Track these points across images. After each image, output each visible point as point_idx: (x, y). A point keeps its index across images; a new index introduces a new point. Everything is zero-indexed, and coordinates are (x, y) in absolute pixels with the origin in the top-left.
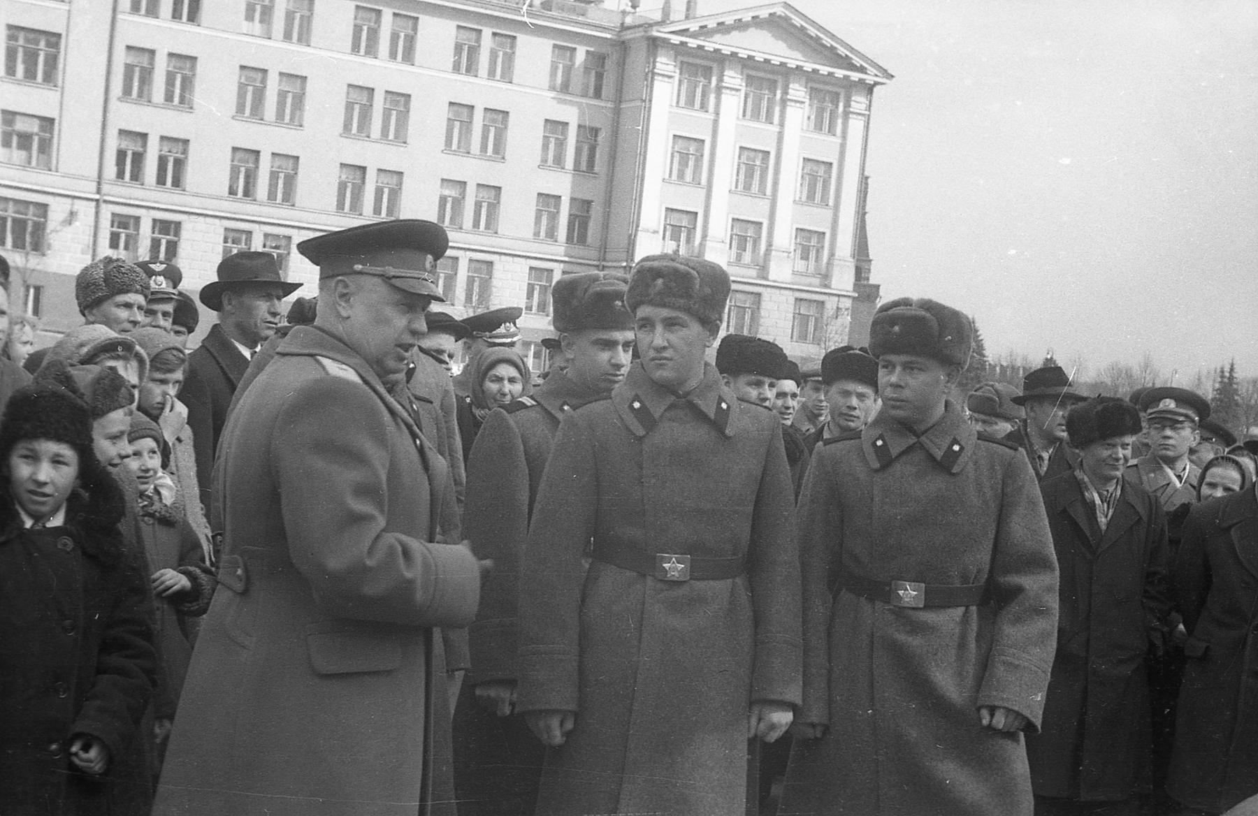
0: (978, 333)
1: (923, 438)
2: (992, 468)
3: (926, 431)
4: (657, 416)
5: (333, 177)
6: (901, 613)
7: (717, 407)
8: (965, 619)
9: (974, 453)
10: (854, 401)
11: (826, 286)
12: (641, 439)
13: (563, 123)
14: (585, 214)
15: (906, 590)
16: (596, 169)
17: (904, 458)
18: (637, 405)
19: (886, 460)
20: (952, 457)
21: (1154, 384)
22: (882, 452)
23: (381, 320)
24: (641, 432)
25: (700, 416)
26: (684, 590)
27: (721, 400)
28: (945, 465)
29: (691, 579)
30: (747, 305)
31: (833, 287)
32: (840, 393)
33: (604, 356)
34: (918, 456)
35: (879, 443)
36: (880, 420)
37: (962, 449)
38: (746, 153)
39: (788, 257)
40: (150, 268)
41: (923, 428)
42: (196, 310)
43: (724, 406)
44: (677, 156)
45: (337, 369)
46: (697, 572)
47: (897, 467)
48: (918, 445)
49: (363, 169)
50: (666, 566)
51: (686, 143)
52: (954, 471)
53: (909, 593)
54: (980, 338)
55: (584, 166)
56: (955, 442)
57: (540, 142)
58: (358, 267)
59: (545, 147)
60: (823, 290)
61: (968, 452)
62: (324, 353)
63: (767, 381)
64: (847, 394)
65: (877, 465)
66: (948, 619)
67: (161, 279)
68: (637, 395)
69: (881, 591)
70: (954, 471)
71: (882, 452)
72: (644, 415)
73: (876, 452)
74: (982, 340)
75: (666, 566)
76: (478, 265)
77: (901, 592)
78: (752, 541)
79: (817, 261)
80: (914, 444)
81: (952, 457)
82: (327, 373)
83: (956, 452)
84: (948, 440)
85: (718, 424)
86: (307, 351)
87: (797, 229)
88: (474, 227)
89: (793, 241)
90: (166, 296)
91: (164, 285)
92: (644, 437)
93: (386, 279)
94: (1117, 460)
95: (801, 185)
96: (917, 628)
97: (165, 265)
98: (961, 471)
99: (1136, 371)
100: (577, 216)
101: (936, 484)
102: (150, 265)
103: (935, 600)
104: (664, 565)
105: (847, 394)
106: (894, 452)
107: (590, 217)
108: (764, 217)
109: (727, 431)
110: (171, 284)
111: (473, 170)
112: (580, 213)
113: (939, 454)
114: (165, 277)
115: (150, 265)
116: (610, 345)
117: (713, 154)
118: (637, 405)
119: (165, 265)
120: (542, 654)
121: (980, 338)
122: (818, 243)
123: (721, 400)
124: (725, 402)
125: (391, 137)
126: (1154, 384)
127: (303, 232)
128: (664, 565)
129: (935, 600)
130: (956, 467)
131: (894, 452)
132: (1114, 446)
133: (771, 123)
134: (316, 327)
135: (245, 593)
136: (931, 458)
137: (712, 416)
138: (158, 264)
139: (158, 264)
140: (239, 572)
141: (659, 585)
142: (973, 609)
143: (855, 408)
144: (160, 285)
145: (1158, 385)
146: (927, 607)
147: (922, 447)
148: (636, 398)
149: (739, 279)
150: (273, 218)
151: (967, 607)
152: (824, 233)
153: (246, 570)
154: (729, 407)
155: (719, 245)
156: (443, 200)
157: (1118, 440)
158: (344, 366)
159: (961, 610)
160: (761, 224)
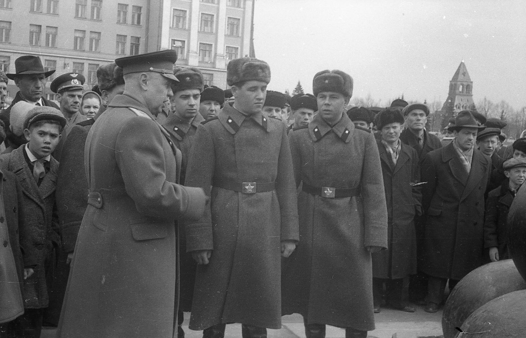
0: (302, 87)
1: (333, 128)
2: (361, 140)
3: (334, 126)
4: (239, 125)
5: (27, 30)
6: (326, 200)
7: (262, 121)
8: (350, 202)
9: (353, 134)
10: (307, 116)
11: (214, 68)
12: (233, 135)
13: (126, 5)
14: (137, 43)
15: (328, 190)
16: (141, 24)
17: (326, 137)
18: (230, 121)
19: (319, 137)
20: (345, 136)
21: (372, 105)
22: (317, 134)
23: (160, 91)
24: (233, 132)
25: (256, 124)
26: (254, 197)
27: (263, 117)
28: (343, 139)
29: (256, 192)
30: (208, 79)
31: (216, 67)
32: (301, 113)
33: (185, 102)
34: (331, 136)
35: (316, 130)
36: (314, 121)
37: (349, 132)
38: (205, 15)
39: (223, 58)
40: (70, 76)
41: (334, 123)
42: (53, 92)
43: (265, 120)
44: (175, 17)
45: (140, 113)
46: (258, 189)
47: (323, 141)
48: (331, 131)
49: (40, 26)
50: (247, 187)
51: (207, 16)
52: (346, 142)
53: (329, 192)
54: (302, 89)
55: (136, 23)
56: (346, 129)
57: (116, 13)
58: (151, 69)
59: (119, 15)
60: (213, 69)
61: (351, 134)
62: (132, 106)
63: (274, 108)
64: (304, 113)
65: (316, 139)
66: (343, 202)
67: (76, 80)
68: (229, 117)
69: (317, 191)
70: (346, 142)
71: (317, 134)
72: (233, 125)
73: (343, 133)
74: (303, 90)
75: (247, 187)
76: (77, 65)
77: (326, 192)
78: (278, 175)
79: (209, 56)
80: (330, 130)
81: (345, 136)
82: (137, 115)
83: (347, 134)
84: (344, 129)
85: (263, 128)
86: (124, 106)
87: (227, 47)
88: (90, 49)
89: (225, 52)
90: (78, 88)
91: (78, 83)
92: (235, 134)
93: (162, 73)
94: (391, 134)
95: (228, 28)
96: (333, 207)
97: (77, 74)
98: (349, 142)
99: (365, 101)
100: (134, 44)
101: (339, 147)
102: (71, 75)
103: (339, 194)
104: (246, 187)
105: (304, 113)
106: (323, 134)
107: (139, 44)
108: (239, 46)
109: (268, 130)
110: (80, 83)
111: (86, 25)
112: (134, 43)
113: (340, 135)
114: (78, 80)
115: (71, 75)
116: (187, 97)
117: (190, 16)
118: (230, 121)
119: (77, 74)
120: (197, 227)
121: (302, 89)
122: (236, 52)
123: (263, 117)
124: (265, 118)
125: (95, 18)
126: (372, 105)
127: (19, 54)
128: (246, 187)
129: (339, 194)
130: (347, 140)
131: (323, 134)
132: (389, 128)
133: (240, 8)
134: (124, 95)
135: (102, 208)
136: (337, 136)
137: (261, 124)
138: (74, 74)
139: (74, 74)
140: (99, 199)
141: (244, 196)
142: (354, 198)
143: (308, 120)
144: (76, 83)
145: (373, 106)
146: (336, 197)
147: (333, 132)
148: (230, 118)
149: (203, 68)
150: (7, 49)
151: (352, 197)
152: (238, 48)
153: (102, 198)
154: (266, 120)
155: (195, 54)
156: (76, 39)
157: (389, 125)
158: (143, 112)
159: (349, 198)
160: (211, 45)
